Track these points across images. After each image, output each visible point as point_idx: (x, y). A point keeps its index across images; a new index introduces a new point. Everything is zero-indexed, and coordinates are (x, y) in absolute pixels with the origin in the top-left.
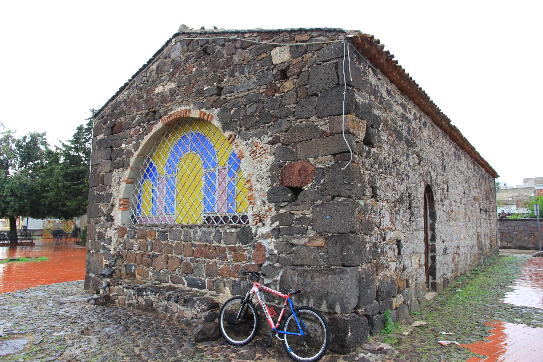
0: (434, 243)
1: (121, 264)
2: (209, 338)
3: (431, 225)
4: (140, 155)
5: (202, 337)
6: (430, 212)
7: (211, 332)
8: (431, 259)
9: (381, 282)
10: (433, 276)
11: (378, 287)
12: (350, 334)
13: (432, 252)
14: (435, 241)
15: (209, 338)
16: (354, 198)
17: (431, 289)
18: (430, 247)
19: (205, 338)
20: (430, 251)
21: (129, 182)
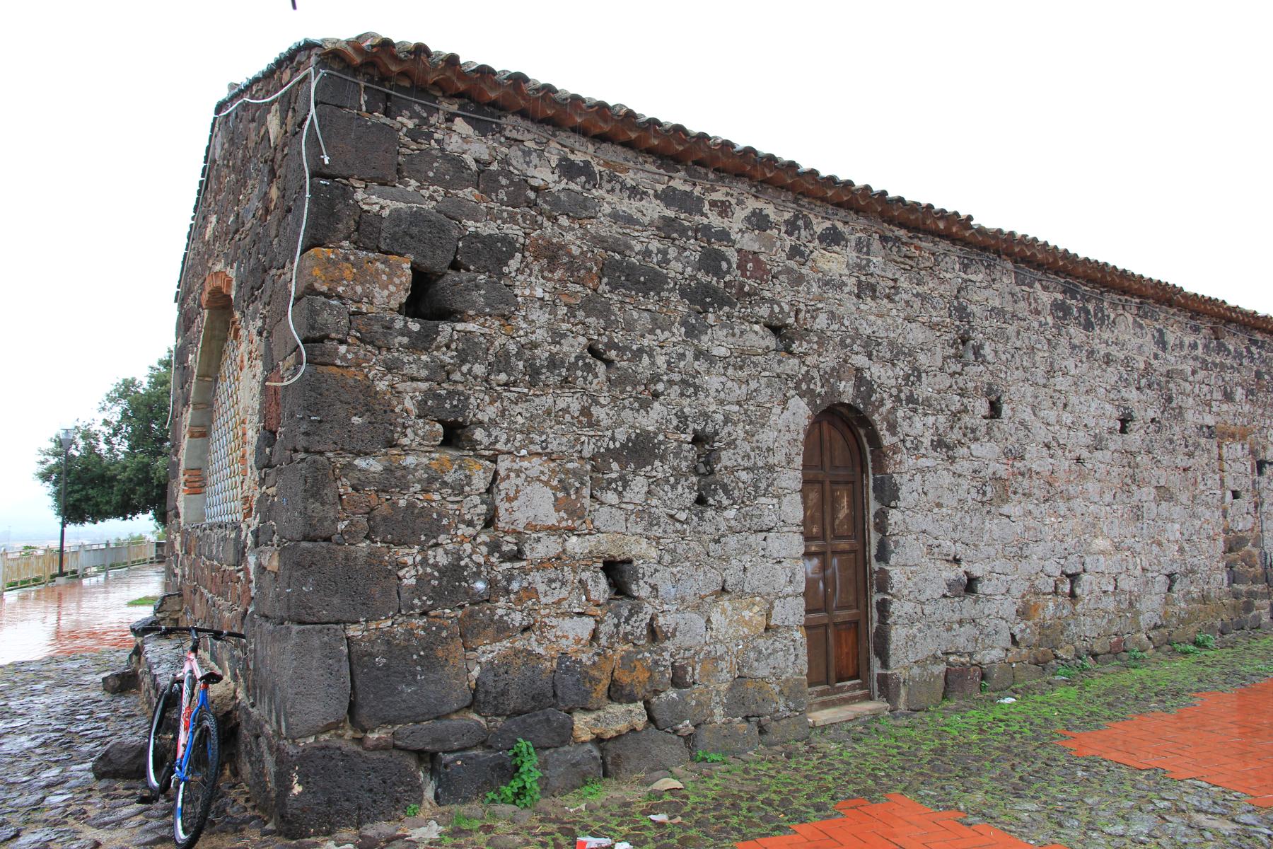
0: (883, 566)
1: (177, 608)
2: (117, 770)
3: (876, 515)
4: (204, 376)
5: (104, 769)
6: (875, 480)
7: (125, 759)
8: (878, 609)
9: (490, 668)
10: (880, 658)
11: (477, 680)
12: (297, 789)
13: (879, 591)
14: (887, 562)
15: (117, 770)
16: (330, 455)
17: (877, 693)
18: (875, 576)
19: (109, 772)
20: (875, 589)
21: (196, 434)
